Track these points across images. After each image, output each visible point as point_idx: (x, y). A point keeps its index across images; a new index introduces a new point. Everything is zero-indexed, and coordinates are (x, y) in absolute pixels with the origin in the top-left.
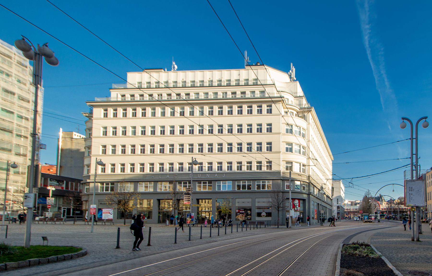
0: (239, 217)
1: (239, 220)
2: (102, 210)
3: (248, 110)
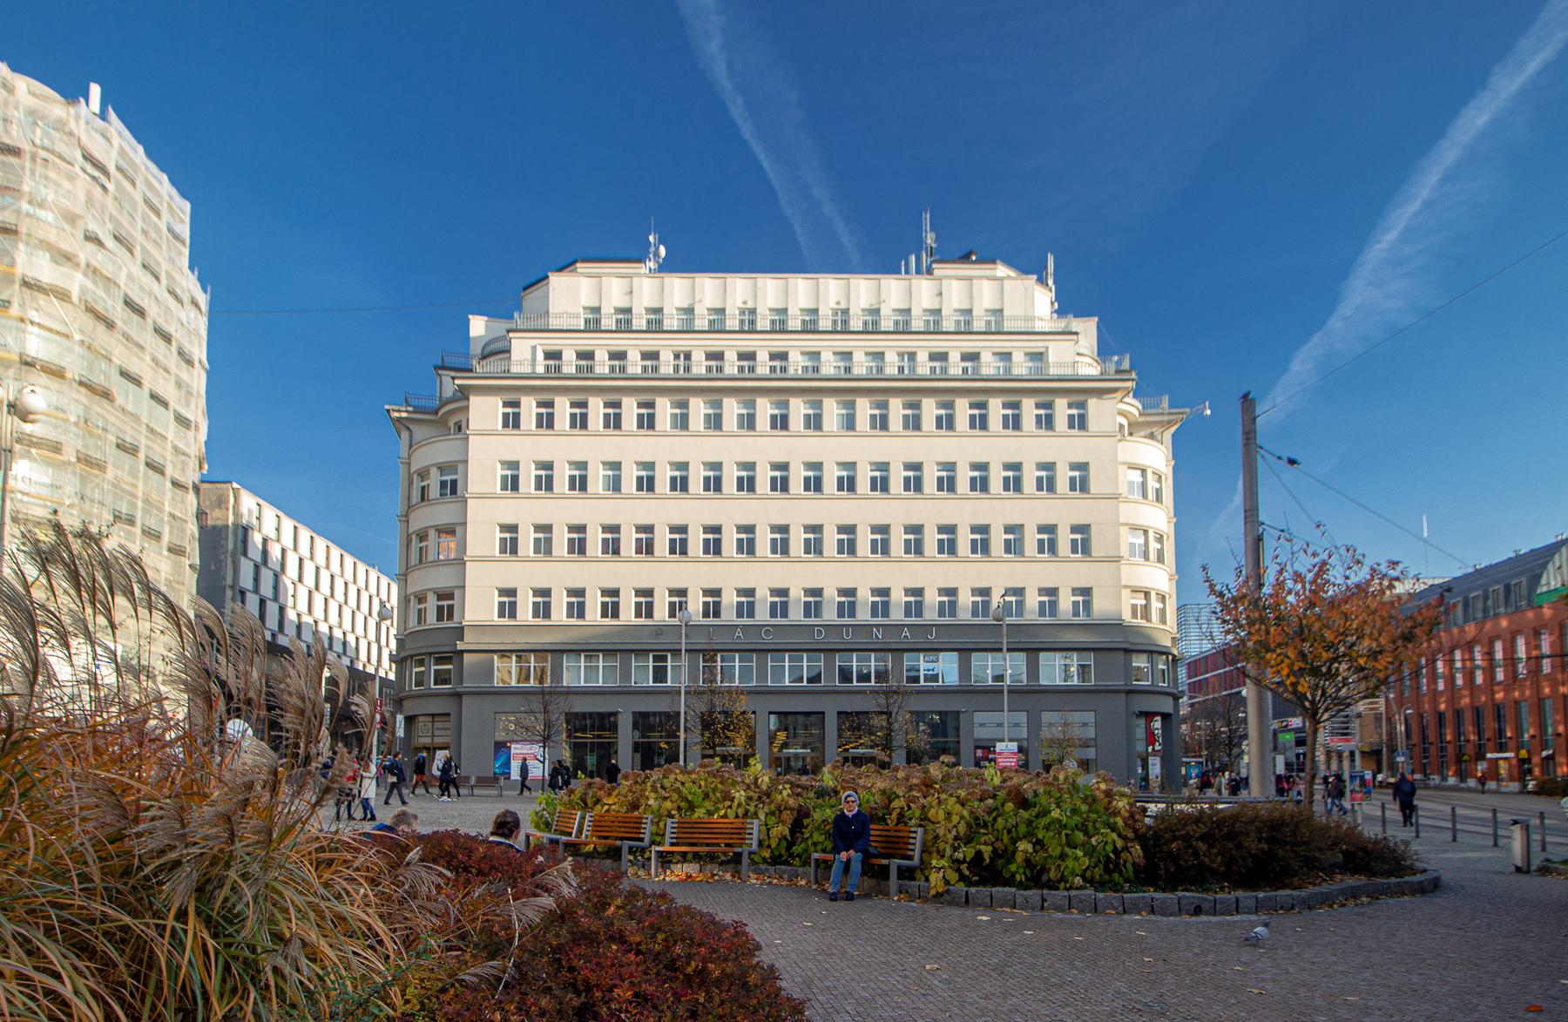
3: (573, 416)
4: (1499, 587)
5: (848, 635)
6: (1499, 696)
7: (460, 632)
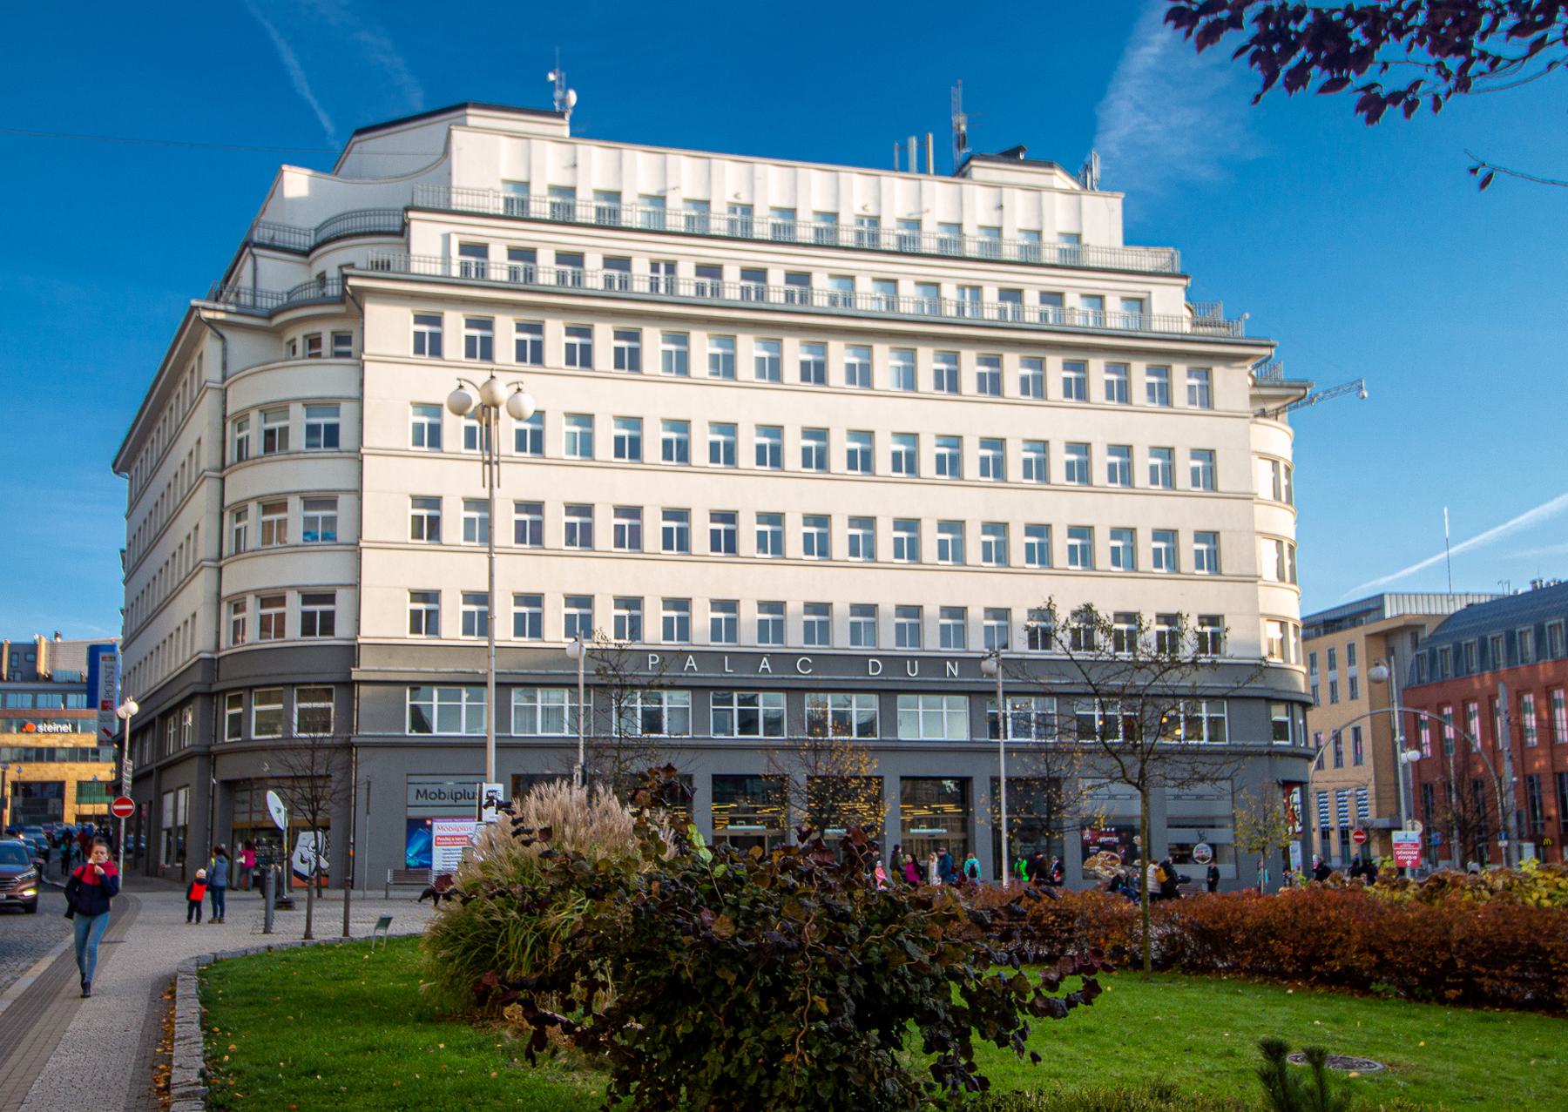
0: (1095, 863)
1: (1096, 877)
2: (430, 827)
5: (913, 672)
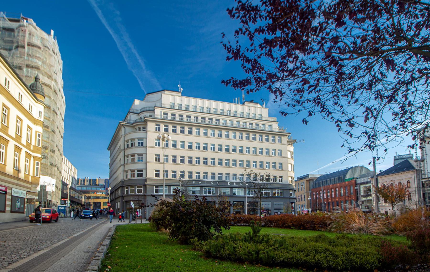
4: (337, 177)
6: (337, 199)
7: (145, 180)
